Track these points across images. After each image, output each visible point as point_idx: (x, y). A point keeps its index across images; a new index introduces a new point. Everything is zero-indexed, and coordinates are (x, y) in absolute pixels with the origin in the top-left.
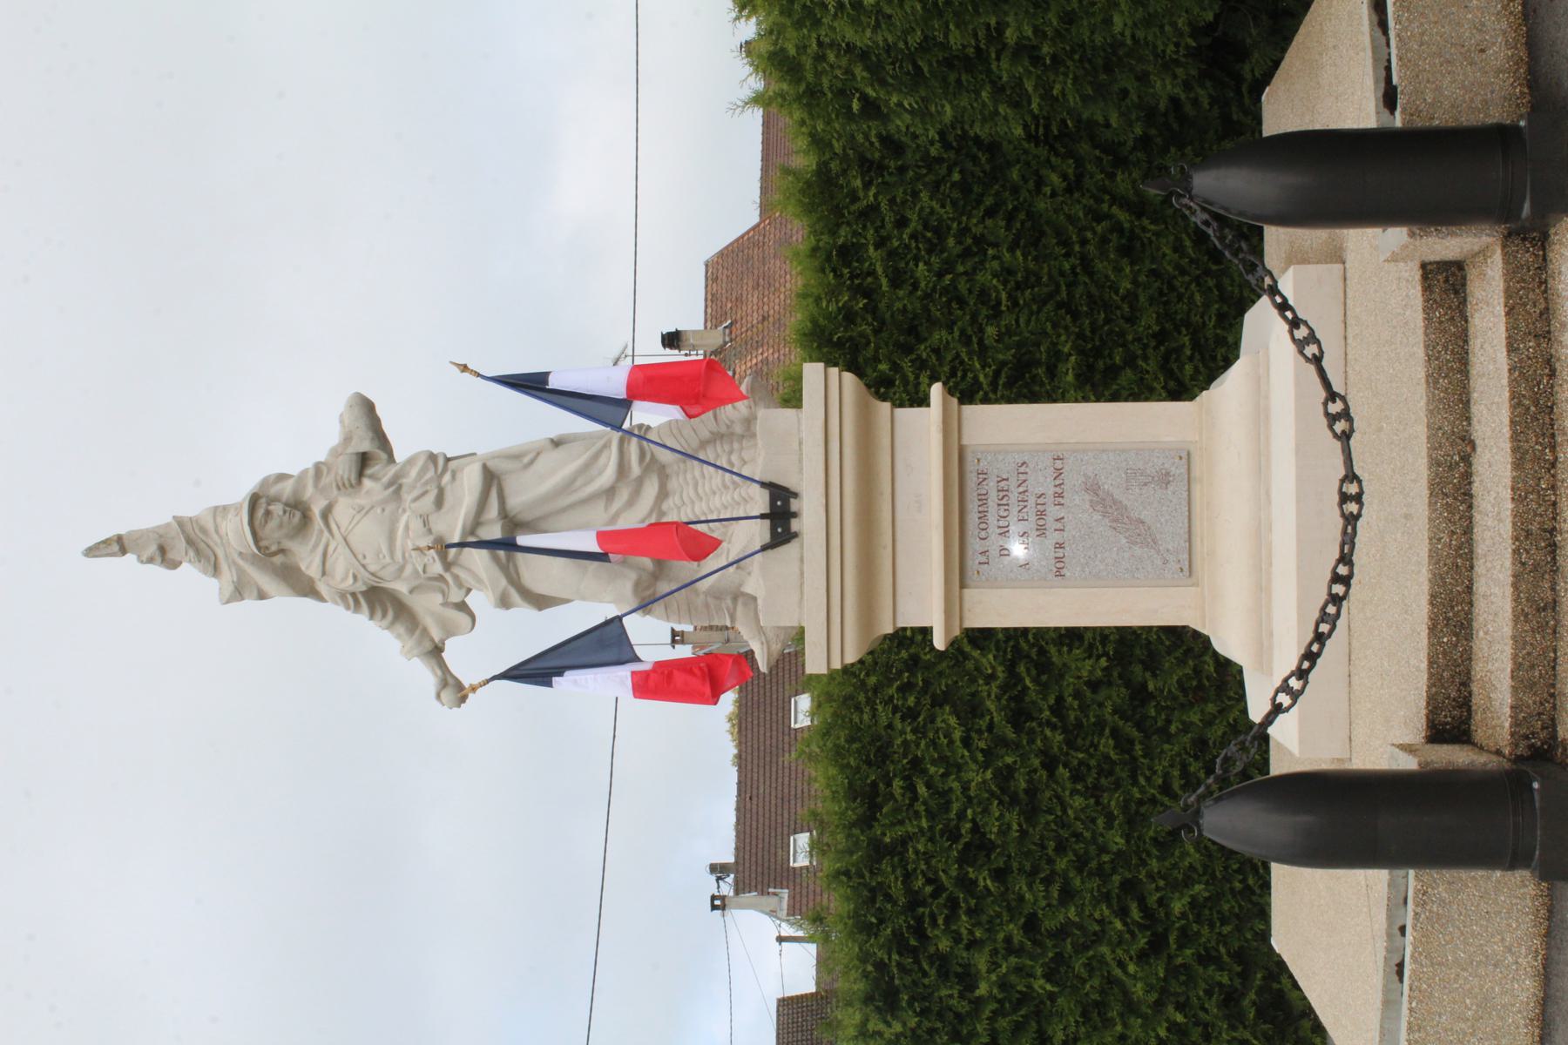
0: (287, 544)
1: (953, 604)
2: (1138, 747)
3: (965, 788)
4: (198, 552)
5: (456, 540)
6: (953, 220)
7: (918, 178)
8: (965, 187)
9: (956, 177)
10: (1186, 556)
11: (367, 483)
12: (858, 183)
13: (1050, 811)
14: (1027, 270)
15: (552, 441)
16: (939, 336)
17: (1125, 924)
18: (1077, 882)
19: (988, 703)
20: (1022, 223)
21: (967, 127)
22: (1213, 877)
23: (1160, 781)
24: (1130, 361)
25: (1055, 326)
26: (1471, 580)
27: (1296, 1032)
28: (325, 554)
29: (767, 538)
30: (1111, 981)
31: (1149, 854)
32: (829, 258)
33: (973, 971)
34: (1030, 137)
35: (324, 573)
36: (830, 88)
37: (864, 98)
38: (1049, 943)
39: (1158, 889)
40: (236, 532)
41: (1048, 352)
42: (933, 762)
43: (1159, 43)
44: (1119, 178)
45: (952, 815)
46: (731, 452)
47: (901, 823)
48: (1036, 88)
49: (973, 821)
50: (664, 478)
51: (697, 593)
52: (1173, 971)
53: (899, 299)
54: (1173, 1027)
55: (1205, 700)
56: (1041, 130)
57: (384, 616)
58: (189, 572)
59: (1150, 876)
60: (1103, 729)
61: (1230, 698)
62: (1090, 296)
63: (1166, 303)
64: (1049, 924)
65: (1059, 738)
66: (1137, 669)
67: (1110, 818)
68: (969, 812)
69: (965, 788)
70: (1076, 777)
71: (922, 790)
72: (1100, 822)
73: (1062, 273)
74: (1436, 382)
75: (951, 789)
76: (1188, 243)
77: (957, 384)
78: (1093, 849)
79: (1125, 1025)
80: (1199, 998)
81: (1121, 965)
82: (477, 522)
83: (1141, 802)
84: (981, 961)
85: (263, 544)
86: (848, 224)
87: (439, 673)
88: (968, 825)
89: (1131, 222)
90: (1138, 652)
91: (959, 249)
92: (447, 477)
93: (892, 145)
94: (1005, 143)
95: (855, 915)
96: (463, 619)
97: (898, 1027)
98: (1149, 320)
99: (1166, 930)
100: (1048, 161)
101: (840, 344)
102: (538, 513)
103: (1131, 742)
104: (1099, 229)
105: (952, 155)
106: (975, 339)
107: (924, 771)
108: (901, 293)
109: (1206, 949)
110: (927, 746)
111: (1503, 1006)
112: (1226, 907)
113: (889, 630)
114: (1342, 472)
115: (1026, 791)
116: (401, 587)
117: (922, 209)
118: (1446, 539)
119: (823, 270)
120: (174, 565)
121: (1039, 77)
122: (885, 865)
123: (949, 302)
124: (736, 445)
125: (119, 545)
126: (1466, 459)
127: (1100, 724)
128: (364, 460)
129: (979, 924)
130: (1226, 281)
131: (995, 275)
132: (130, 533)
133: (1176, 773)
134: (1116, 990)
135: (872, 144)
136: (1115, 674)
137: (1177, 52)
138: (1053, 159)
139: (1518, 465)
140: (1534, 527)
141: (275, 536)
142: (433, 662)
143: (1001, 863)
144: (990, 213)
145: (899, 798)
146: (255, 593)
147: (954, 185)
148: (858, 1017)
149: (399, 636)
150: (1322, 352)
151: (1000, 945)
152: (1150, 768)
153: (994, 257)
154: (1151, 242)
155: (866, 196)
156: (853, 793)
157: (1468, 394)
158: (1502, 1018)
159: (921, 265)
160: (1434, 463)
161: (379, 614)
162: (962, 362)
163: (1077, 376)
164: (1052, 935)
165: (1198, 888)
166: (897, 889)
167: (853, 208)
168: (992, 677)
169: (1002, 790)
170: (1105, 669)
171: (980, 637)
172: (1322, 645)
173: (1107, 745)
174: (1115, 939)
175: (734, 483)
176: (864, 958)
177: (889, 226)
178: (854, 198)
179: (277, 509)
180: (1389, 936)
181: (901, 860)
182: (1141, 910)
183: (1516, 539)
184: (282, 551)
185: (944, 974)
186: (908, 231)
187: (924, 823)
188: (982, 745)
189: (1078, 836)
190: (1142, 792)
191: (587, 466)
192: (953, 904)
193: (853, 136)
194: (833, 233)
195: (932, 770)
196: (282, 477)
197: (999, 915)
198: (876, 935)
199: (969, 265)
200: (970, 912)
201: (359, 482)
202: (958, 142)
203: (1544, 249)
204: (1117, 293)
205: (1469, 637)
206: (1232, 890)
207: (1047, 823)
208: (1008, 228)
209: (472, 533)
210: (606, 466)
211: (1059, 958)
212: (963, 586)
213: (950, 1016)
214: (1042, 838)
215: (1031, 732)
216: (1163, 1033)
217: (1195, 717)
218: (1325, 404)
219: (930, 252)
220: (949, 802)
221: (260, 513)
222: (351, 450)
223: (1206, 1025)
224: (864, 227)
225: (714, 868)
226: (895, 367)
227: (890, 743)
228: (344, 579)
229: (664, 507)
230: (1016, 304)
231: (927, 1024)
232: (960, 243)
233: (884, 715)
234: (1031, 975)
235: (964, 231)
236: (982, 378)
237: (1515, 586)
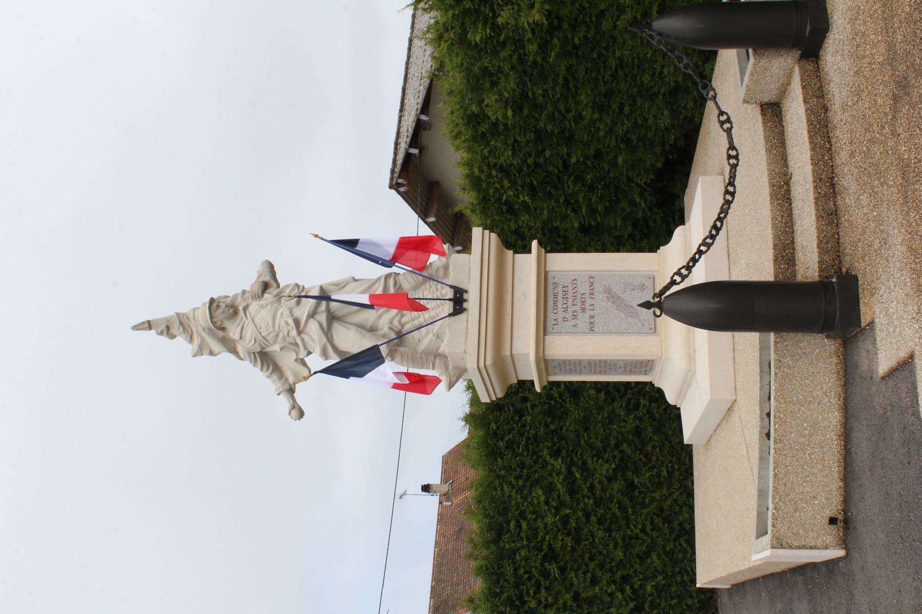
4: (184, 328)
11: (266, 295)
13: (587, 540)
22: (667, 574)
26: (793, 238)
28: (242, 328)
29: (451, 311)
35: (241, 338)
38: (585, 607)
40: (203, 317)
57: (268, 369)
65: (591, 501)
66: (629, 473)
70: (600, 522)
71: (524, 525)
72: (611, 546)
74: (770, 151)
75: (538, 527)
83: (631, 538)
85: (214, 320)
90: (630, 465)
99: (644, 603)
111: (824, 427)
114: (728, 146)
118: (780, 219)
120: (173, 337)
122: (505, 563)
125: (149, 325)
126: (787, 183)
127: (611, 499)
128: (266, 286)
133: (648, 523)
139: (813, 149)
140: (823, 177)
143: (562, 563)
145: (513, 531)
146: (208, 351)
156: (490, 528)
157: (786, 156)
158: (823, 435)
160: (772, 185)
161: (265, 367)
180: (761, 418)
183: (815, 182)
187: (525, 543)
189: (601, 553)
192: (538, 586)
195: (530, 516)
196: (227, 297)
200: (548, 589)
201: (263, 295)
203: (817, 63)
205: (794, 265)
206: (676, 582)
212: (545, 334)
221: (215, 305)
228: (250, 341)
237: (816, 203)
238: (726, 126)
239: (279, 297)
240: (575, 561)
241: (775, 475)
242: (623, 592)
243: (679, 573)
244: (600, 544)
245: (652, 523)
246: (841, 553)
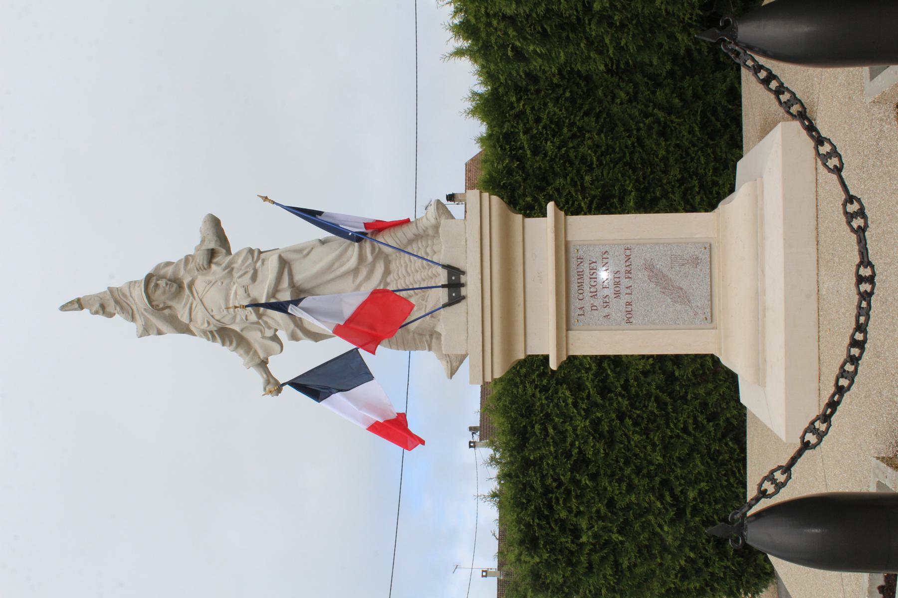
0: (170, 303)
2: (670, 407)
3: (575, 430)
4: (122, 308)
5: (263, 301)
6: (566, 118)
7: (547, 95)
8: (572, 100)
9: (568, 94)
10: (709, 310)
11: (213, 267)
12: (514, 99)
14: (607, 145)
15: (320, 241)
16: (559, 182)
17: (662, 503)
18: (636, 481)
19: (587, 383)
20: (605, 119)
21: (573, 66)
22: (711, 477)
23: (682, 426)
24: (665, 195)
25: (623, 176)
27: (755, 561)
28: (191, 309)
30: (654, 534)
31: (675, 465)
32: (498, 140)
33: (579, 527)
34: (609, 71)
35: (191, 320)
36: (496, 43)
37: (514, 48)
38: (621, 514)
39: (680, 485)
40: (138, 297)
41: (619, 189)
42: (557, 416)
43: (681, 14)
44: (658, 93)
45: (568, 444)
46: (427, 247)
47: (539, 448)
48: (611, 41)
49: (579, 448)
51: (408, 331)
52: (688, 529)
53: (537, 161)
54: (689, 560)
55: (707, 382)
56: (614, 67)
57: (231, 344)
59: (677, 478)
60: (650, 397)
61: (720, 380)
62: (642, 159)
63: (685, 163)
64: (621, 504)
65: (626, 402)
67: (654, 445)
68: (577, 443)
69: (575, 430)
70: (636, 424)
71: (551, 431)
72: (649, 448)
73: (627, 147)
76: (697, 129)
77: (569, 208)
78: (645, 462)
79: (662, 558)
80: (703, 544)
81: (660, 526)
82: (276, 290)
83: (671, 437)
84: (584, 524)
85: (154, 303)
86: (509, 121)
87: (265, 376)
88: (576, 451)
89: (665, 117)
91: (569, 134)
92: (259, 263)
93: (532, 78)
94: (594, 76)
95: (515, 497)
96: (276, 346)
97: (537, 560)
98: (675, 172)
100: (619, 85)
101: (504, 187)
102: (313, 283)
103: (666, 404)
104: (647, 122)
105: (565, 82)
106: (579, 183)
107: (553, 420)
108: (538, 158)
109: (707, 517)
110: (554, 407)
112: (718, 495)
113: (521, 356)
114: (857, 260)
115: (608, 431)
116: (237, 328)
117: (549, 113)
119: (495, 147)
120: (111, 315)
121: (612, 35)
122: (531, 472)
123: (564, 163)
124: (430, 242)
125: (79, 304)
129: (582, 503)
130: (718, 150)
131: (589, 148)
132: (85, 297)
133: (691, 421)
134: (657, 539)
135: (521, 76)
136: (657, 367)
137: (691, 19)
138: (621, 84)
141: (161, 298)
142: (261, 370)
144: (587, 114)
146: (155, 331)
147: (566, 99)
148: (516, 552)
149: (241, 355)
150: (842, 164)
151: (594, 515)
152: (676, 419)
153: (589, 138)
154: (676, 129)
155: (518, 106)
156: (513, 431)
159: (549, 143)
161: (228, 343)
162: (572, 196)
163: (636, 203)
164: (622, 509)
165: (703, 484)
166: (537, 485)
167: (511, 113)
169: (595, 430)
170: (652, 365)
172: (841, 396)
173: (652, 406)
174: (657, 512)
175: (428, 265)
176: (519, 521)
177: (531, 122)
178: (512, 108)
179: (162, 283)
181: (540, 468)
182: (671, 497)
184: (169, 307)
185: (563, 529)
186: (542, 124)
187: (552, 449)
188: (584, 406)
189: (636, 455)
190: (672, 431)
191: (340, 256)
192: (568, 492)
193: (510, 73)
194: (501, 127)
195: (557, 420)
196: (168, 264)
197: (593, 498)
198: (526, 509)
199: (576, 142)
200: (577, 497)
202: (568, 74)
204: (657, 157)
206: (721, 485)
207: (620, 449)
208: (597, 122)
209: (274, 296)
210: (352, 256)
211: (626, 522)
212: (568, 329)
213: (566, 552)
214: (617, 457)
215: (611, 399)
216: (683, 563)
217: (701, 391)
218: (844, 205)
219: (554, 136)
220: (565, 437)
221: (152, 285)
222: (204, 248)
223: (706, 559)
224: (518, 123)
225: (471, 429)
226: (535, 199)
227: (533, 405)
228: (203, 324)
229: (388, 280)
230: (601, 163)
231: (554, 557)
232: (571, 131)
234: (611, 531)
235: (572, 124)
236: (583, 204)
238: (857, 222)
239: (230, 269)
243: (725, 475)
244: (636, 446)
245: (695, 421)
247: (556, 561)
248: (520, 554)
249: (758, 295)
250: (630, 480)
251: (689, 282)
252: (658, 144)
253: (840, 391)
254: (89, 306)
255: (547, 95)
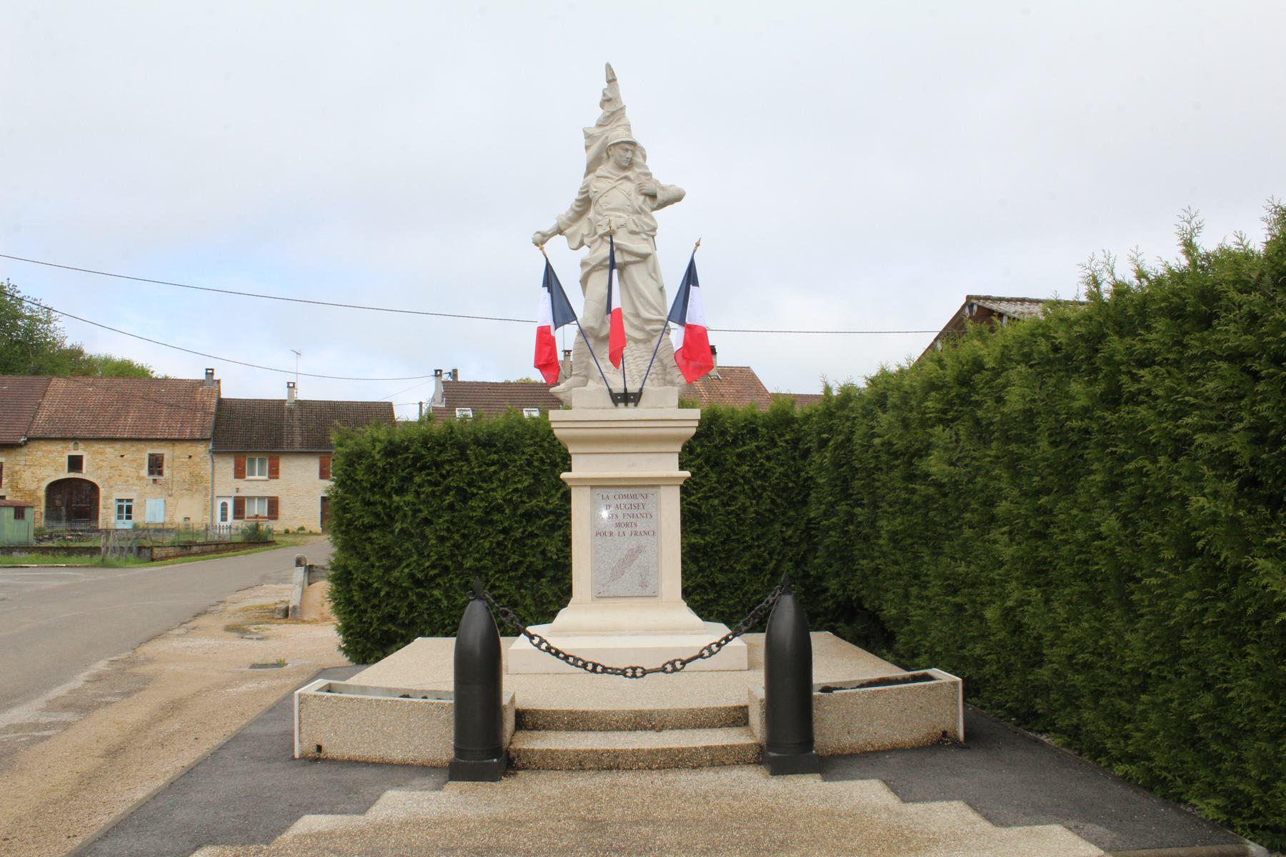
0: (612, 160)
1: (582, 482)
3: (493, 490)
7: (790, 467)
9: (790, 485)
11: (642, 198)
12: (787, 437)
18: (448, 544)
24: (701, 570)
30: (400, 560)
34: (809, 521)
37: (828, 440)
40: (617, 135)
50: (646, 341)
58: (599, 113)
59: (451, 579)
64: (428, 530)
66: (551, 573)
67: (479, 560)
69: (493, 490)
70: (499, 544)
71: (492, 469)
81: (408, 566)
82: (622, 250)
84: (410, 497)
93: (806, 454)
95: (431, 437)
97: (377, 457)
98: (721, 578)
101: (709, 428)
103: (516, 570)
107: (501, 470)
116: (591, 214)
120: (602, 106)
122: (456, 451)
125: (612, 80)
126: (653, 728)
139: (650, 752)
140: (620, 760)
141: (616, 153)
143: (457, 507)
144: (773, 501)
156: (491, 435)
160: (651, 713)
165: (445, 603)
166: (444, 456)
168: (548, 503)
171: (567, 497)
173: (515, 558)
176: (411, 441)
178: (780, 435)
179: (629, 155)
180: (422, 691)
185: (403, 479)
189: (470, 544)
192: (437, 484)
196: (644, 157)
200: (433, 493)
202: (807, 486)
205: (567, 730)
211: (411, 536)
212: (592, 487)
215: (521, 522)
216: (375, 585)
225: (455, 371)
226: (698, 456)
233: (529, 450)
235: (764, 489)
238: (669, 667)
239: (640, 212)
240: (461, 520)
241: (352, 700)
242: (433, 566)
246: (297, 756)
247: (375, 473)
248: (379, 441)
249: (617, 631)
250: (448, 539)
251: (628, 583)
252: (745, 563)
253: (566, 658)
254: (609, 89)
255: (790, 467)
